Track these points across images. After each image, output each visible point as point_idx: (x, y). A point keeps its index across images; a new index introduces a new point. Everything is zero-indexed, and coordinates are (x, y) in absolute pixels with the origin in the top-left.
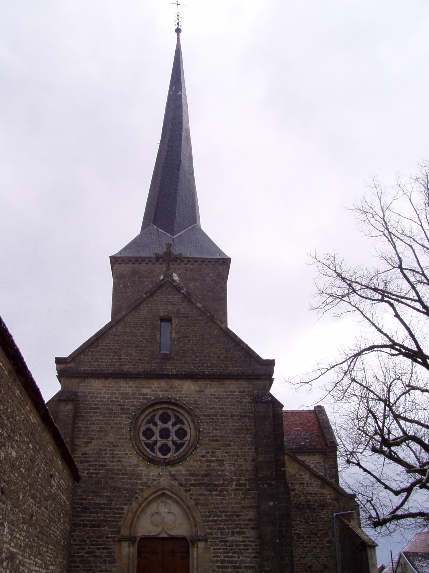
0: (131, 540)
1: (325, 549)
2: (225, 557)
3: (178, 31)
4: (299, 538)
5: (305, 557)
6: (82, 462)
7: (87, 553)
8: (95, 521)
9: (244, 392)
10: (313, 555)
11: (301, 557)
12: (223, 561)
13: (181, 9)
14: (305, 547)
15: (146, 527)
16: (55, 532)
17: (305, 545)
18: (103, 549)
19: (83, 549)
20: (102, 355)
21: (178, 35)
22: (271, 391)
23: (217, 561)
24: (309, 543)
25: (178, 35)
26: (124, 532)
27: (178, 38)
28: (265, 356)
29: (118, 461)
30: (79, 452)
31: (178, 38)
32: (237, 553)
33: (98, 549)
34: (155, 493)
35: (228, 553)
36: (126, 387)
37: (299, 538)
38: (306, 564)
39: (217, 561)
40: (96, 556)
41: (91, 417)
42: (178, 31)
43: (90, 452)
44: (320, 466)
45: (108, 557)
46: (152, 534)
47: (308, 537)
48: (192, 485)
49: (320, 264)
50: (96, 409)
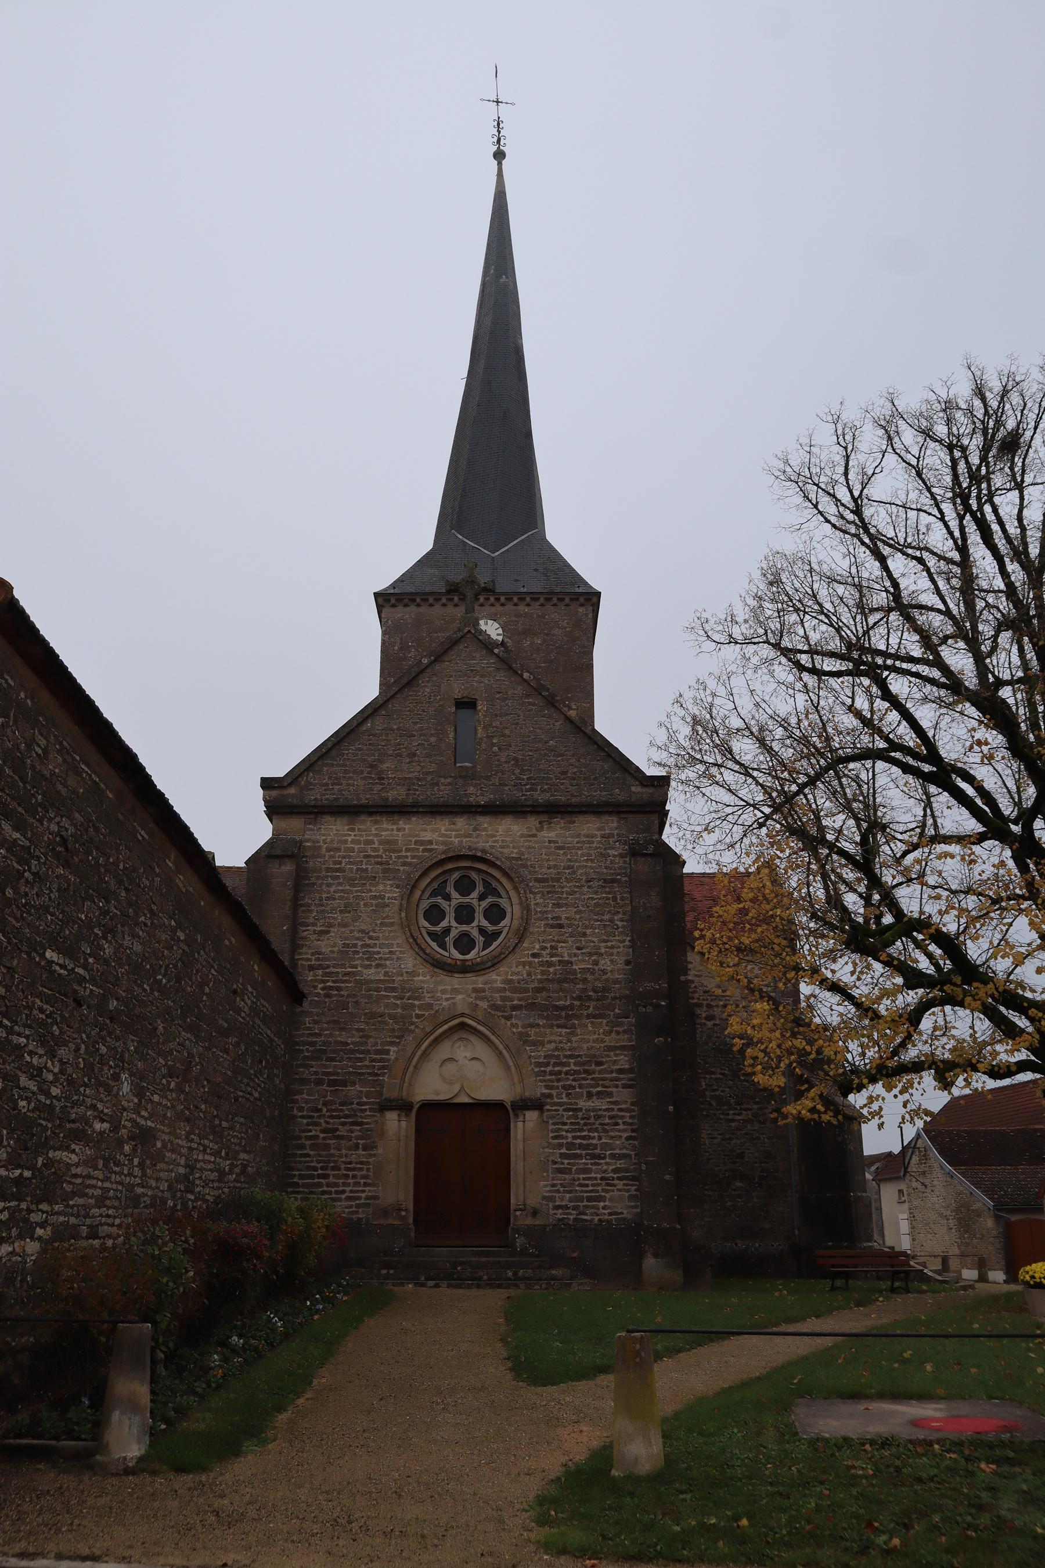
1: (768, 1124)
3: (499, 155)
5: (731, 1139)
10: (746, 1134)
11: (724, 1139)
14: (732, 1120)
17: (730, 1117)
21: (500, 164)
24: (739, 1114)
25: (500, 164)
42: (499, 155)
47: (737, 1104)
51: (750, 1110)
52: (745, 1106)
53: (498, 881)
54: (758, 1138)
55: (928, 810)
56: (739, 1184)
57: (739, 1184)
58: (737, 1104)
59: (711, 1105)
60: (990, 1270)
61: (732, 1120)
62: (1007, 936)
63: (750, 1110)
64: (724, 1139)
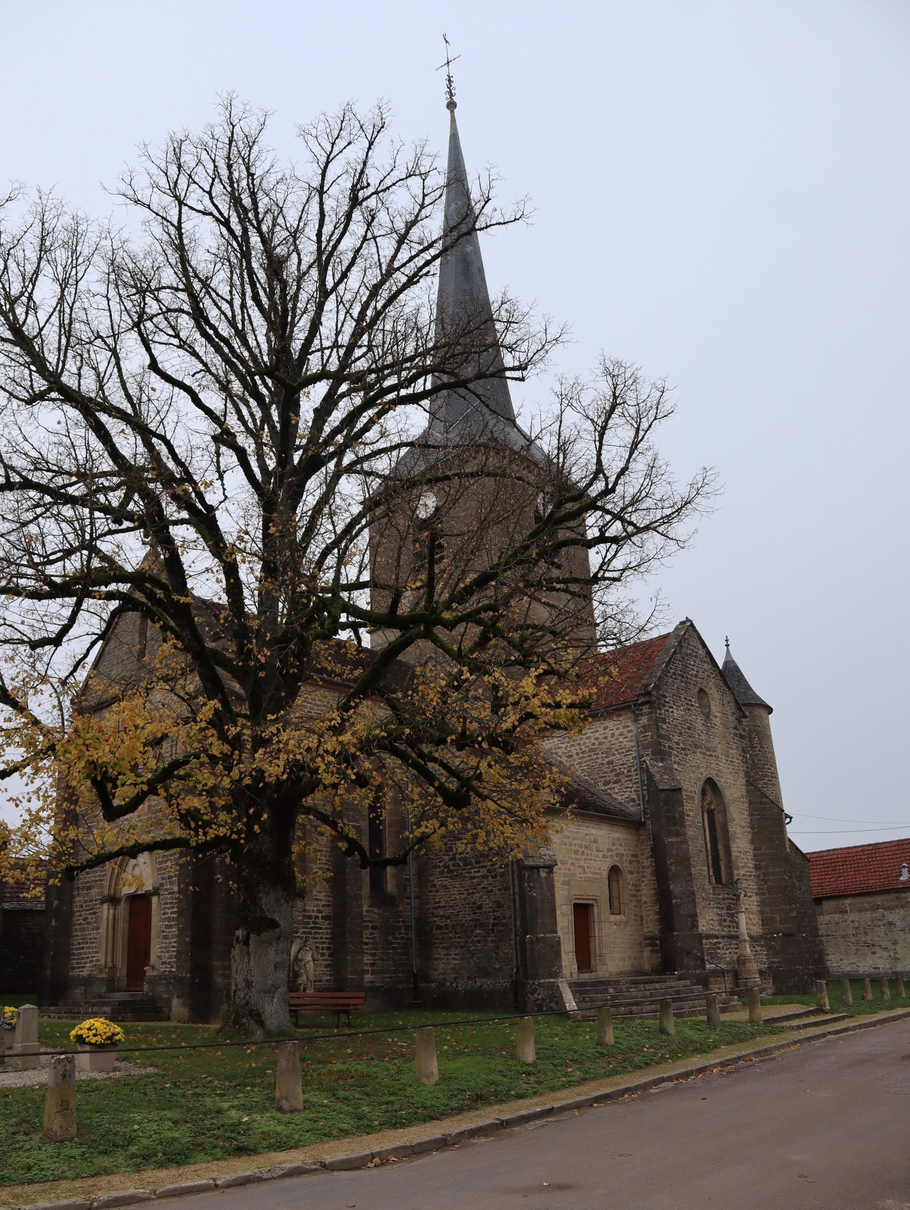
0: (113, 900)
1: (498, 878)
3: (452, 105)
4: (466, 864)
5: (473, 893)
10: (484, 888)
11: (468, 894)
13: (454, 69)
14: (474, 878)
17: (473, 875)
21: (452, 112)
22: (808, 833)
24: (479, 872)
25: (452, 112)
27: (453, 120)
28: (787, 810)
31: (453, 120)
37: (466, 864)
38: (474, 903)
42: (452, 105)
47: (477, 863)
49: (376, 257)
51: (485, 867)
52: (481, 864)
53: (108, 919)
54: (492, 891)
55: (104, 418)
56: (478, 931)
57: (478, 931)
58: (477, 863)
59: (459, 866)
60: (371, 591)
61: (474, 878)
62: (43, 332)
63: (485, 867)
64: (468, 894)
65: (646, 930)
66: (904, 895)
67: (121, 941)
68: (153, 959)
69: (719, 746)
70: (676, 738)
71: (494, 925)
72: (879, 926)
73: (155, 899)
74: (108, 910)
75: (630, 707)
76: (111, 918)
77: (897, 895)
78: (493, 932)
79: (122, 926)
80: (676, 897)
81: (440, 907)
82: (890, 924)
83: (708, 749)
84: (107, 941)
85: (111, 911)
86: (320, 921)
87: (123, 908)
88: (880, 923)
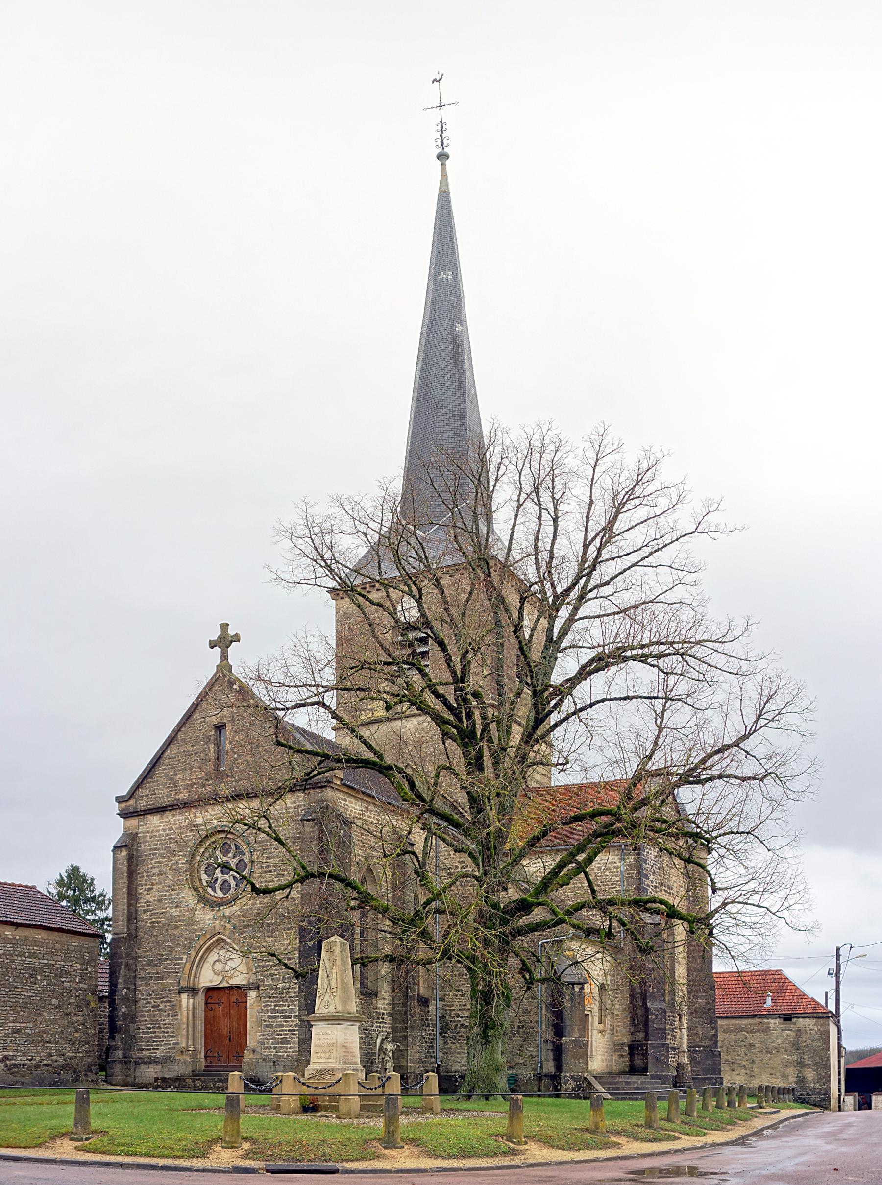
0: (193, 991)
2: (275, 1006)
3: (443, 157)
6: (145, 911)
7: (153, 1007)
8: (158, 973)
9: (299, 806)
12: (273, 1011)
15: (207, 978)
16: (54, 991)
18: (166, 1002)
19: (149, 1003)
20: (158, 785)
21: (443, 164)
23: (268, 1011)
25: (443, 164)
26: (184, 984)
29: (176, 907)
30: (142, 900)
32: (286, 1001)
33: (162, 1002)
34: (211, 938)
35: (278, 1001)
36: (176, 819)
39: (268, 1011)
40: (160, 1010)
41: (152, 859)
42: (443, 157)
43: (151, 900)
44: (615, 867)
45: (170, 1010)
46: (214, 984)
48: (245, 927)
50: (155, 849)
65: (616, 1038)
66: (766, 1021)
67: (201, 1027)
68: (251, 1042)
69: (675, 885)
70: (651, 877)
71: (519, 1027)
72: (740, 1047)
73: (253, 994)
74: (188, 999)
75: (621, 846)
76: (191, 1006)
77: (760, 1020)
78: (518, 1033)
79: (201, 1014)
80: (652, 1014)
81: (465, 1009)
82: (751, 1045)
83: (669, 887)
84: (188, 1027)
85: (191, 1001)
86: (385, 1017)
87: (201, 997)
88: (741, 1044)
